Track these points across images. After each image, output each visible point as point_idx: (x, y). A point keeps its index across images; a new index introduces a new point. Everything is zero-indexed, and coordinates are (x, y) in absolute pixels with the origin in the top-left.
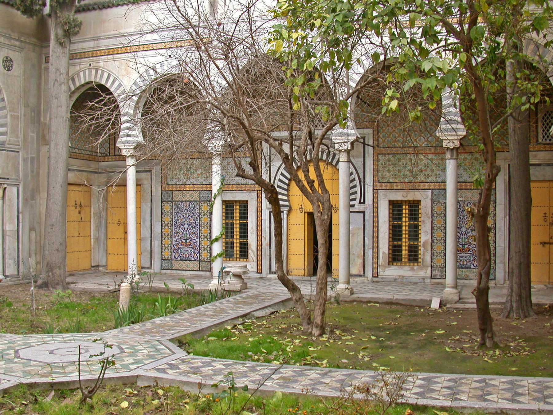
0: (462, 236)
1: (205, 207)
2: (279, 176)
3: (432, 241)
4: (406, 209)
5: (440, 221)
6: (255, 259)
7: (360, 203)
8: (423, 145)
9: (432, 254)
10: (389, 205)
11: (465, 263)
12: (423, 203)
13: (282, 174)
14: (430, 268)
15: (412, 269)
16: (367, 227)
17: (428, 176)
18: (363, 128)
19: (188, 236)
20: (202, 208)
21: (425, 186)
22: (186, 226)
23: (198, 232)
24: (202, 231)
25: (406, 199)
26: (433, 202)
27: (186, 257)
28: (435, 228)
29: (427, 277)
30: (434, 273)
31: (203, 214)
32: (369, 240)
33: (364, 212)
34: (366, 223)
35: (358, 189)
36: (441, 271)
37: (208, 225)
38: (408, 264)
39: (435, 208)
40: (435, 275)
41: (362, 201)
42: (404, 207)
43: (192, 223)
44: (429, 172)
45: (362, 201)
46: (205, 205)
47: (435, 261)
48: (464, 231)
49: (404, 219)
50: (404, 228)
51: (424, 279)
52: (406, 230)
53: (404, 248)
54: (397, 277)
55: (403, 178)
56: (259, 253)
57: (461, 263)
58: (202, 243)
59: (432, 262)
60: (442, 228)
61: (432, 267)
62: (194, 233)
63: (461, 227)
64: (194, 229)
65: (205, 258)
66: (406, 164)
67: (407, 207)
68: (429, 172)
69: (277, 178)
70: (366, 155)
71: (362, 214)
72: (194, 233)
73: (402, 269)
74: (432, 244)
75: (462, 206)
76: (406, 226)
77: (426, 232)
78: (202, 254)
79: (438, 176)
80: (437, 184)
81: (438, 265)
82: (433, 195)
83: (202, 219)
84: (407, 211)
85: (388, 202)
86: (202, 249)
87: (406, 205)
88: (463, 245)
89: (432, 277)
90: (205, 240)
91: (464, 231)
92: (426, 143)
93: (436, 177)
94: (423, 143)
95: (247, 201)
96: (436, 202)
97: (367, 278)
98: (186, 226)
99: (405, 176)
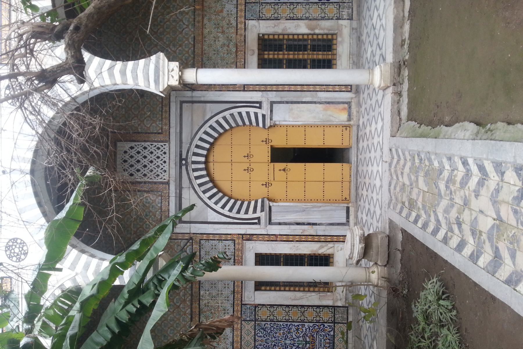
0: (296, 344)
1: (263, 314)
2: (226, 211)
3: (307, 18)
4: (269, 54)
5: (283, 10)
6: (331, 245)
7: (260, 108)
8: (192, 30)
9: (323, 19)
10: (260, 290)
11: (328, 341)
12: (263, 31)
13: (223, 207)
14: (340, 22)
15: (342, 42)
16: (290, 99)
17: (229, 24)
18: (170, 102)
19: (301, 339)
20: (264, 318)
21: (238, 311)
22: (288, 342)
23: (296, 324)
24: (295, 318)
25: (256, 52)
26: (260, 19)
27: (329, 343)
28: (292, 15)
29: (351, 25)
30: (345, 17)
31: (272, 317)
32: (306, 97)
33: (272, 103)
34: (285, 100)
35: (243, 110)
36: (343, 8)
37: (287, 309)
38: (335, 51)
39: (268, 15)
40: (348, 15)
41: (258, 105)
42: (266, 56)
43: (284, 333)
44: (224, 23)
45: (258, 105)
46: (260, 313)
47: (331, 15)
48: (289, 342)
49: (281, 57)
50: (291, 57)
51: (353, 29)
52: (294, 54)
53: (315, 57)
54: (351, 62)
55: (231, 54)
56: (323, 238)
57: (328, 345)
58: (310, 318)
59: (332, 19)
60: (292, 7)
61: (338, 19)
62: (297, 330)
63: (285, 344)
64: (292, 331)
65: (330, 315)
66: (215, 51)
67: (266, 53)
68: (224, 23)
69: (228, 213)
70: (202, 99)
71: (274, 105)
72: (297, 330)
73: (340, 56)
74: (310, 19)
75: (260, 342)
76: (288, 54)
77: (298, 26)
78: (326, 319)
79: (230, 13)
80: (239, 13)
81: (335, 11)
82: (252, 18)
83: (280, 318)
84: (271, 53)
85: (257, 293)
86: (318, 319)
87: (264, 54)
88: (307, 343)
89: (351, 19)
90: (306, 314)
91: (289, 342)
92: (190, 27)
93: (231, 14)
94: (190, 30)
95: (256, 265)
96: (261, 15)
97: (352, 98)
98: (288, 342)
99: (229, 52)
